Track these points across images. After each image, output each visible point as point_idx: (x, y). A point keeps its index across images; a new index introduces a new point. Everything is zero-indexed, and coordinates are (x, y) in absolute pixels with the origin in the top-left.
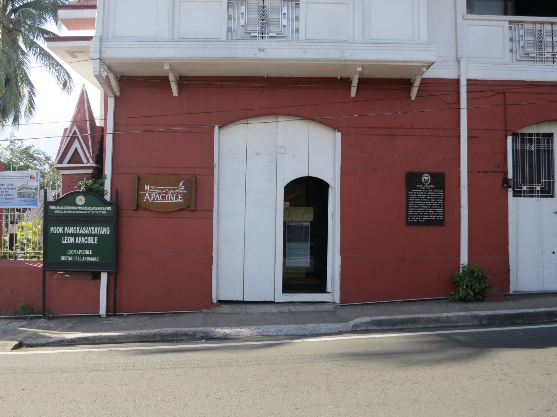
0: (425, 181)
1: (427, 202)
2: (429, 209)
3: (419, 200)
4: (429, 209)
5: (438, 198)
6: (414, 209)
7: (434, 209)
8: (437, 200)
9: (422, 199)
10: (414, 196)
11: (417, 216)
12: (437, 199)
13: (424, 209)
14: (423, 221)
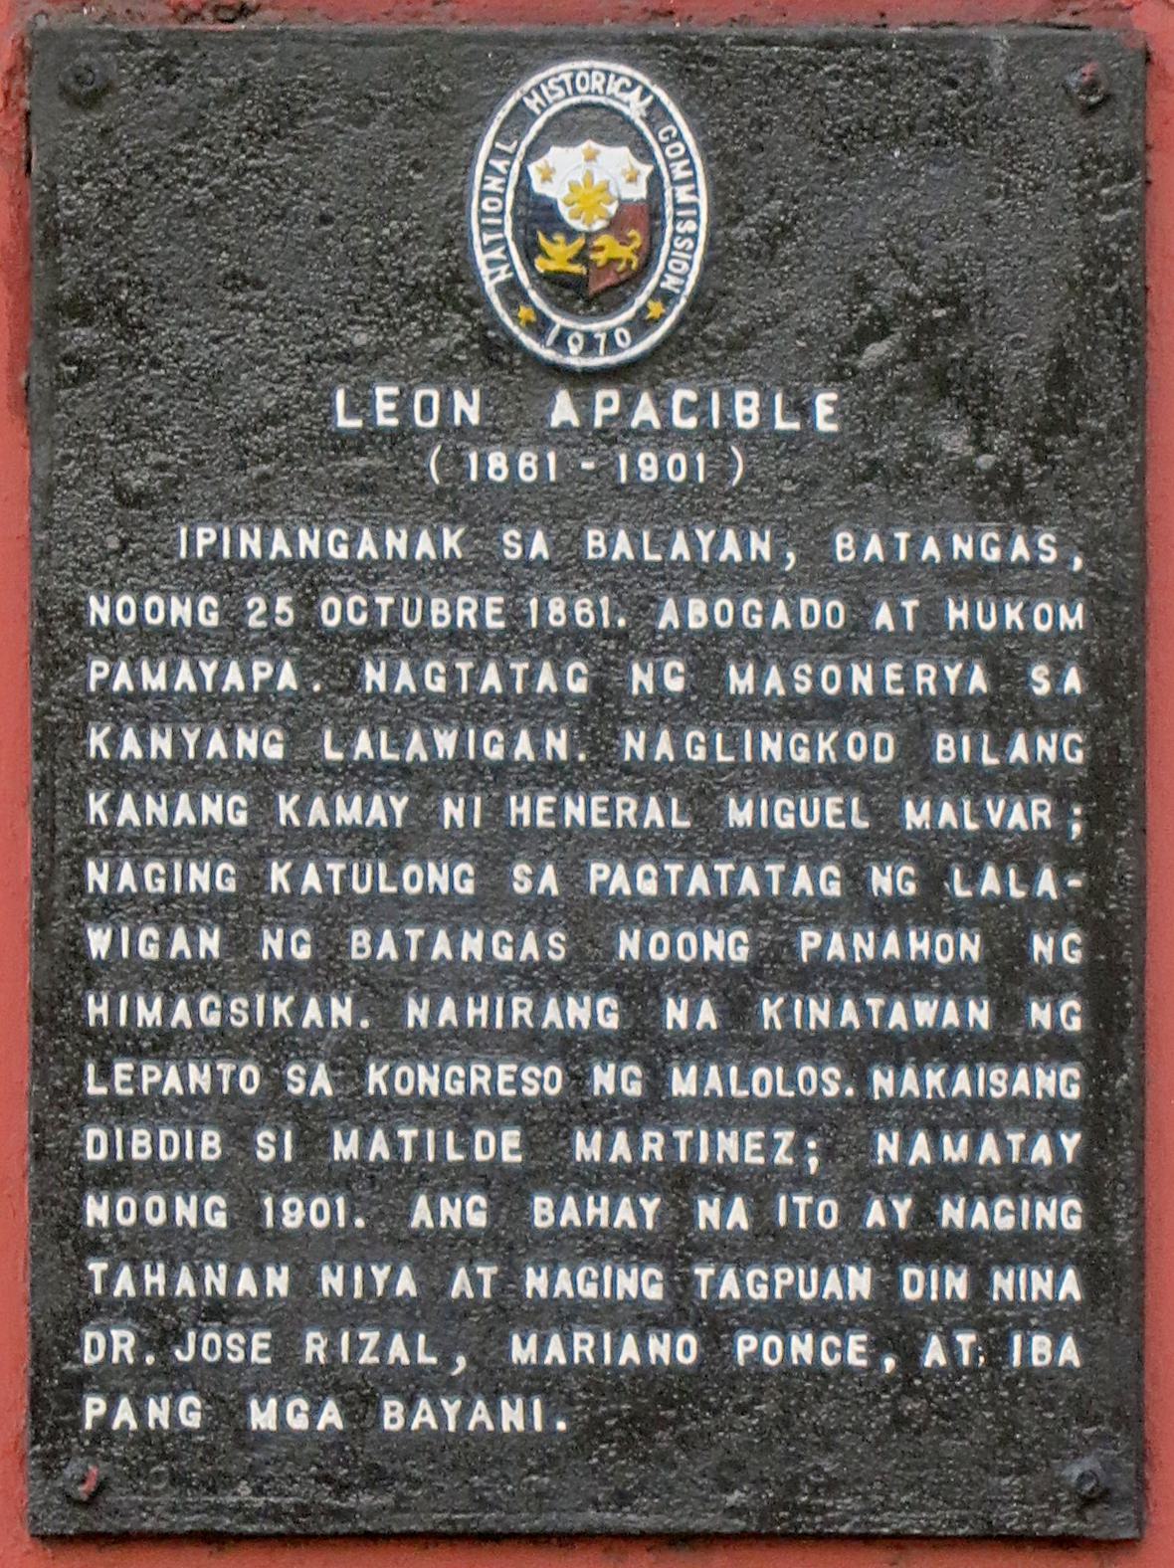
0: (558, 256)
1: (606, 876)
2: (683, 1084)
3: (385, 809)
4: (683, 1084)
5: (945, 747)
6: (250, 1077)
7: (828, 1081)
8: (915, 816)
9: (468, 774)
10: (259, 707)
11: (331, 1281)
12: (926, 778)
13: (545, 1080)
14: (512, 1416)
